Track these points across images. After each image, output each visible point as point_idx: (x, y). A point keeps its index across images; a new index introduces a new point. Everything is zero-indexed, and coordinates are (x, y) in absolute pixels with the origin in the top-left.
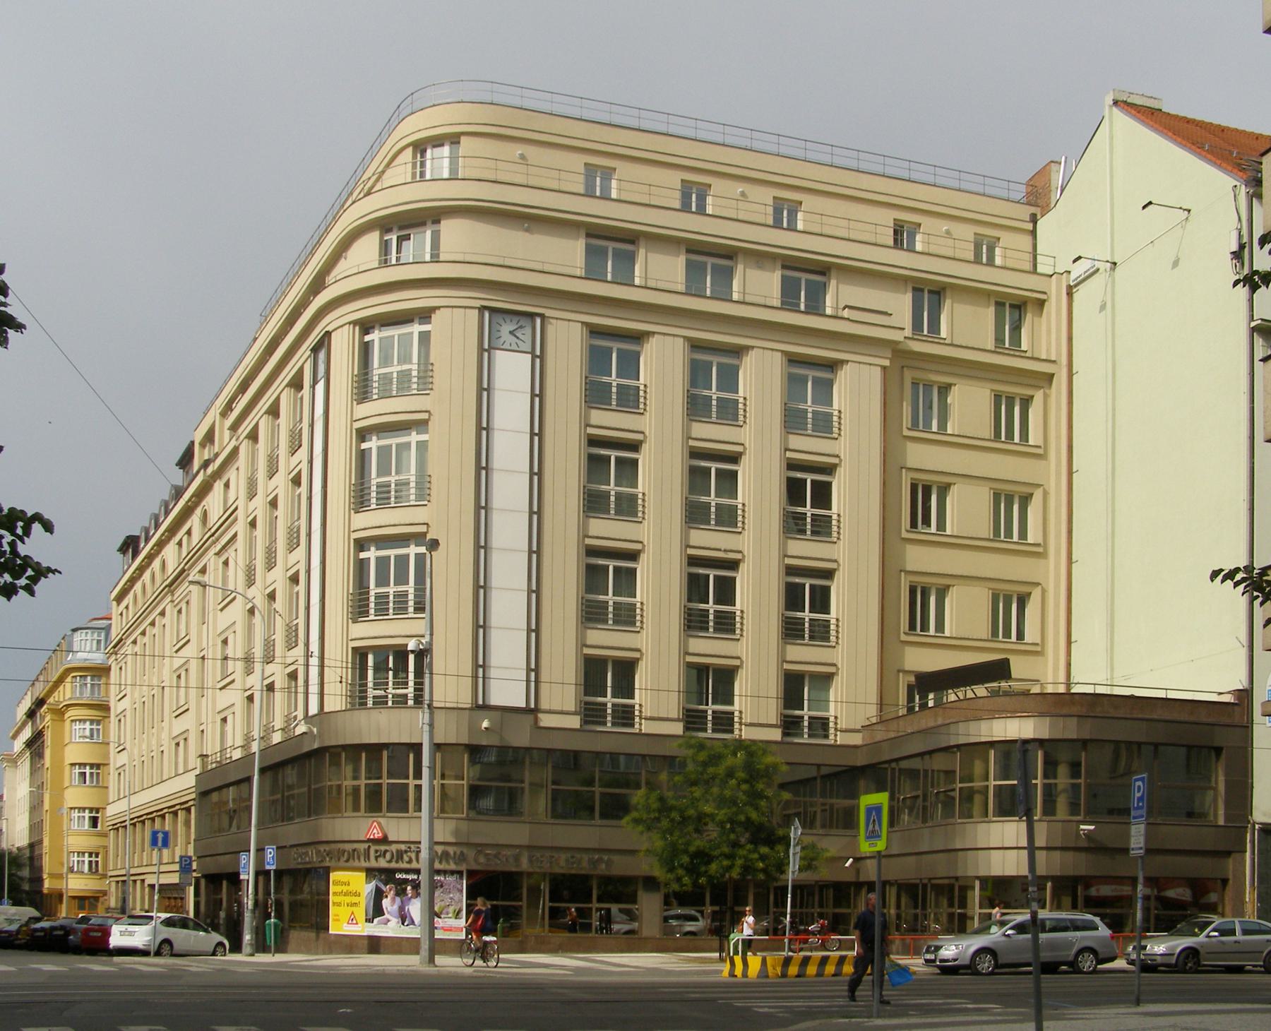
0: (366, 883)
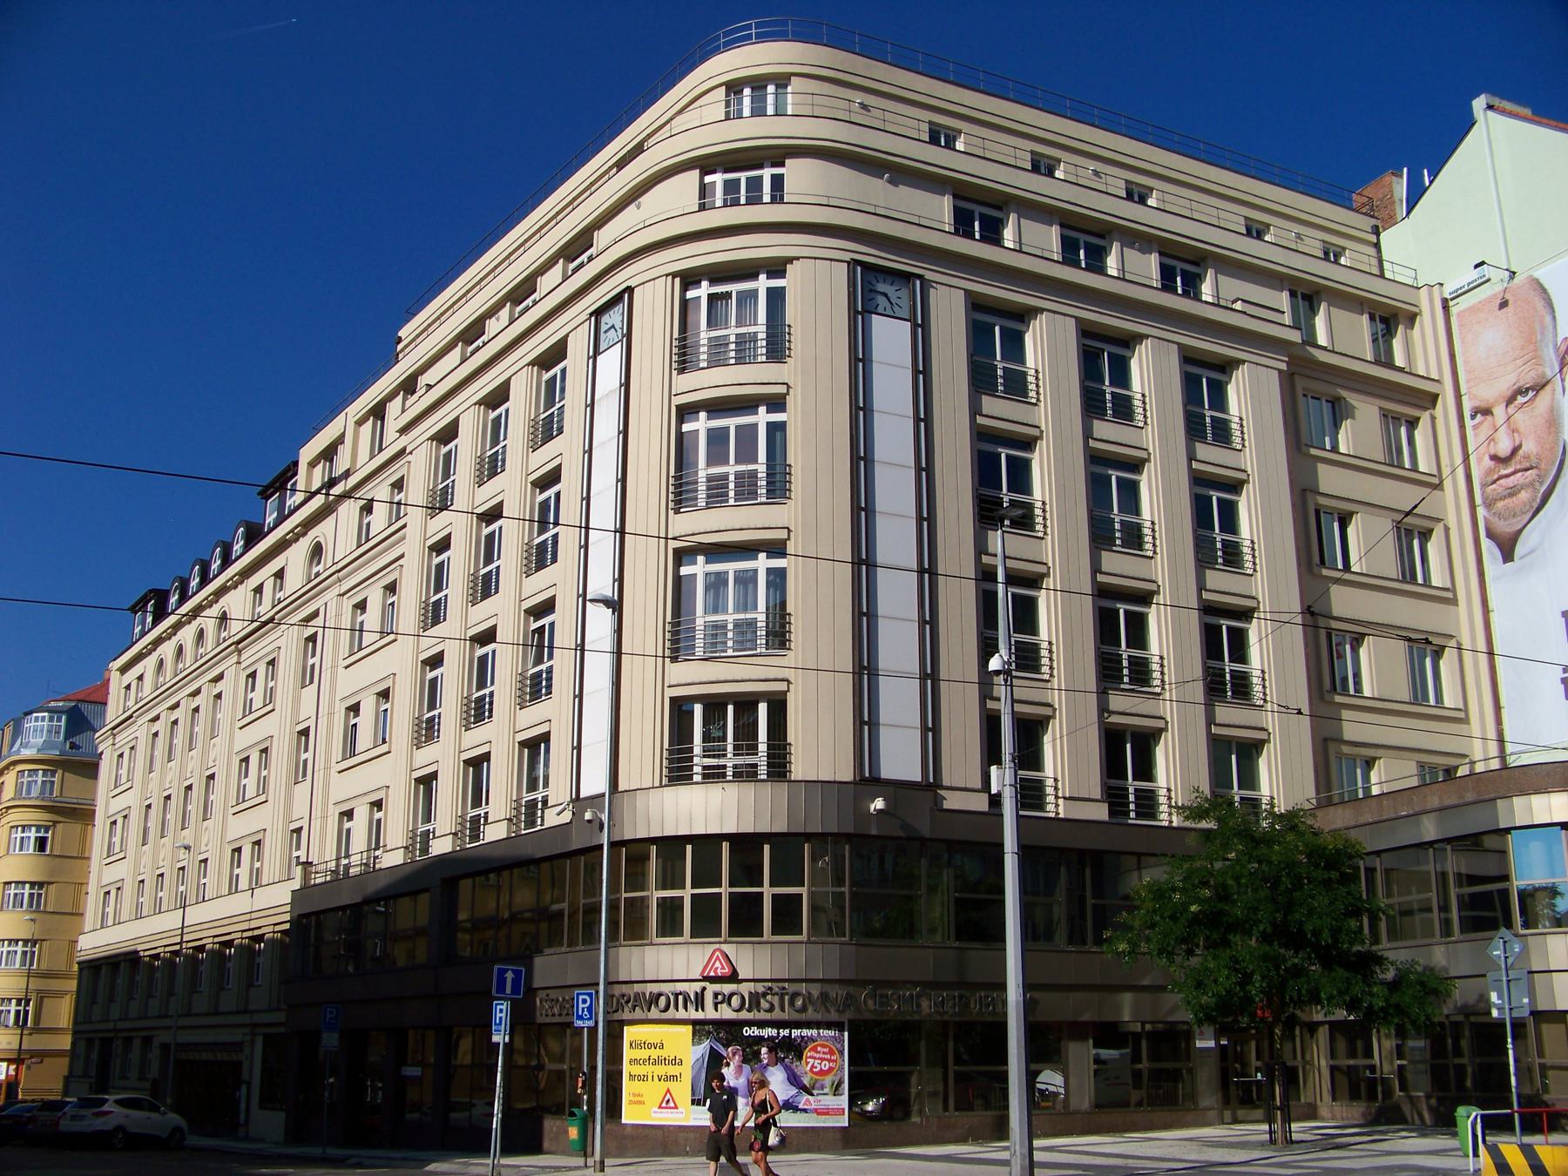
0: (693, 1045)
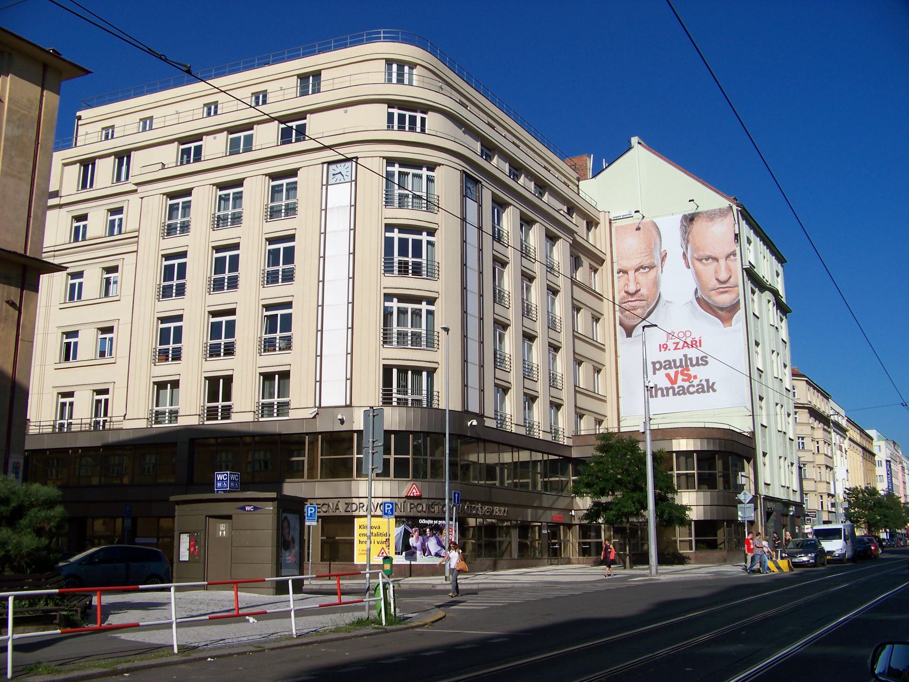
0: (396, 527)
